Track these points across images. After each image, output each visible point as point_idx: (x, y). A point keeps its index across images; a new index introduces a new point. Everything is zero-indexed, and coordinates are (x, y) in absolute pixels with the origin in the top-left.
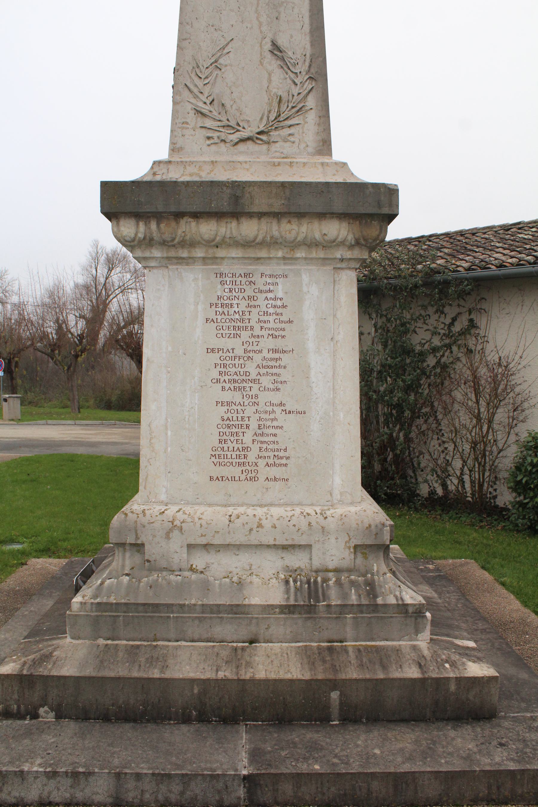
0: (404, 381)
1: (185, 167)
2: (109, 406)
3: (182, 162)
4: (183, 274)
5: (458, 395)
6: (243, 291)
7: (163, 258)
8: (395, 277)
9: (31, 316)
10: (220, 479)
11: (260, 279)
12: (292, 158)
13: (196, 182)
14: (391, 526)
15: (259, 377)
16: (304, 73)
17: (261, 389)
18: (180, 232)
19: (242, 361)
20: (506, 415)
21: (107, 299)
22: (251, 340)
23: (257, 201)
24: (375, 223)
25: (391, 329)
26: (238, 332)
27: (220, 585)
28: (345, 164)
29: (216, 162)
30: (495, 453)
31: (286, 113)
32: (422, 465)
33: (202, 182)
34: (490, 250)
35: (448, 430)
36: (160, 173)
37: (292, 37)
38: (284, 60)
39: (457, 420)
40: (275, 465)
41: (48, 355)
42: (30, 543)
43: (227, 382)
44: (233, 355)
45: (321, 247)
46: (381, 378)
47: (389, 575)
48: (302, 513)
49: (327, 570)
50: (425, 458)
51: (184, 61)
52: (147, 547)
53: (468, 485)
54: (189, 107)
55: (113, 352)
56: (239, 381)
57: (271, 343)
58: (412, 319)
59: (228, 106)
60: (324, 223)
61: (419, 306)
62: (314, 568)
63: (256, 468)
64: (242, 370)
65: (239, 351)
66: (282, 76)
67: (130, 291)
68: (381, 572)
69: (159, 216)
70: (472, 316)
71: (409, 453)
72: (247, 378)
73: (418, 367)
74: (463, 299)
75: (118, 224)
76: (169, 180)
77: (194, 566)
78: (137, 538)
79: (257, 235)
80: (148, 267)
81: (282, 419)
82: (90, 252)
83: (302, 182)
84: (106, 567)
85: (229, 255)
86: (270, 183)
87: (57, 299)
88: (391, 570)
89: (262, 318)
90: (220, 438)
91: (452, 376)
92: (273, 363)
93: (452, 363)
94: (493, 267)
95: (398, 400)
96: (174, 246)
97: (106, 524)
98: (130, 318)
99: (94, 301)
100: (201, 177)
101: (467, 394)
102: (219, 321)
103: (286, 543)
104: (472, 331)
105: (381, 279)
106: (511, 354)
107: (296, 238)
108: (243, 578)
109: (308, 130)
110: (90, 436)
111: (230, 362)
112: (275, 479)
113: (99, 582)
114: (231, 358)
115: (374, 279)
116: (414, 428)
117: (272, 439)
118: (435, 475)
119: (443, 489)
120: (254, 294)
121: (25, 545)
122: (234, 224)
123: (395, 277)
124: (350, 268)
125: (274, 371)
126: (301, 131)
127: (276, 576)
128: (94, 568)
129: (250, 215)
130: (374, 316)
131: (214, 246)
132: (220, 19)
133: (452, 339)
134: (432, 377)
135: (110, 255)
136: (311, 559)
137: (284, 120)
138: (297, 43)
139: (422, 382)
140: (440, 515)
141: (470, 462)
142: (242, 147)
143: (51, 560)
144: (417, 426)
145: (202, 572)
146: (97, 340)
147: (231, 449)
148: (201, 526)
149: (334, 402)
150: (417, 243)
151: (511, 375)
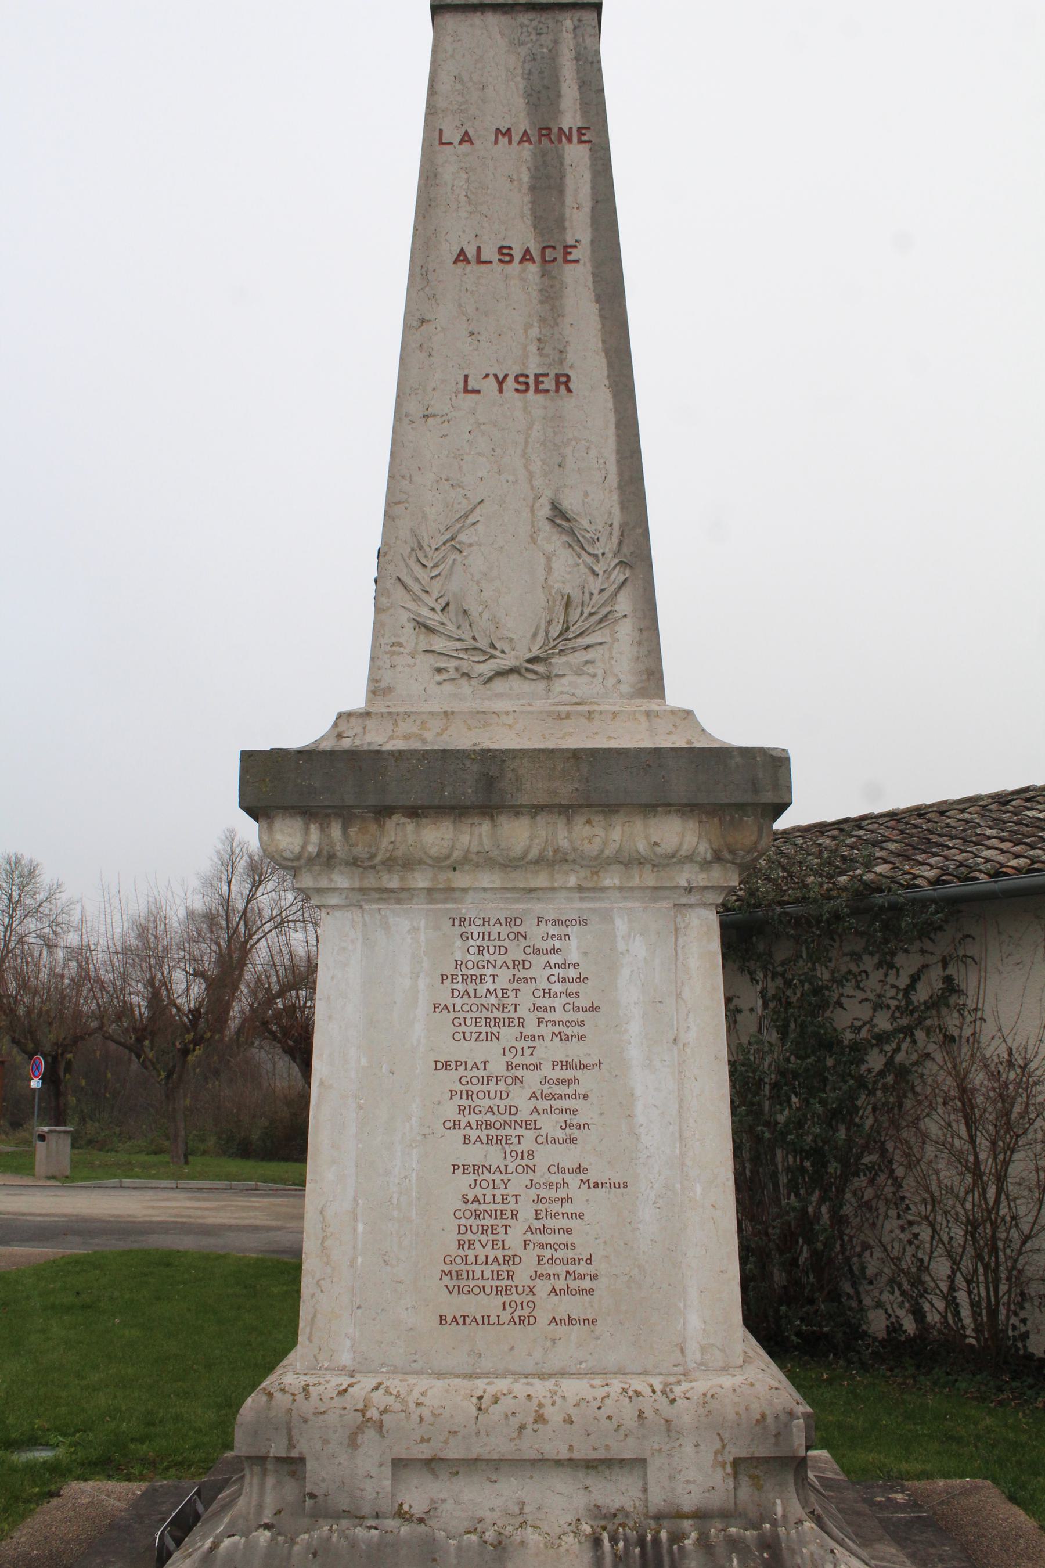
0: (823, 1102)
1: (396, 724)
2: (245, 1151)
3: (390, 713)
4: (391, 920)
5: (932, 1127)
6: (503, 950)
7: (353, 889)
8: (797, 901)
9: (102, 972)
10: (461, 1321)
11: (535, 928)
12: (591, 703)
13: (415, 751)
14: (807, 1416)
15: (535, 1116)
16: (610, 555)
17: (540, 1140)
18: (385, 843)
19: (502, 1086)
20: (1032, 1166)
21: (246, 942)
22: (519, 1045)
23: (528, 784)
24: (749, 820)
25: (794, 999)
26: (495, 1030)
27: (459, 1548)
28: (688, 714)
29: (453, 713)
30: (1016, 1245)
31: (579, 624)
32: (870, 1271)
33: (426, 751)
34: (976, 844)
35: (917, 1199)
36: (350, 733)
37: (586, 495)
38: (574, 533)
39: (934, 1177)
40: (568, 1291)
41: (131, 1050)
42: (70, 1445)
43: (474, 1126)
44: (484, 1073)
45: (649, 866)
46: (779, 1097)
47: (808, 1524)
48: (625, 1390)
49: (681, 1515)
50: (875, 1256)
51: (396, 538)
52: (309, 1466)
53: (965, 1312)
54: (404, 616)
55: (257, 1043)
56: (497, 1125)
57: (557, 1050)
58: (833, 980)
59: (474, 612)
60: (653, 822)
61: (846, 955)
62: (652, 1510)
63: (530, 1298)
64: (502, 1103)
65: (497, 1067)
66: (571, 562)
67: (291, 925)
68: (792, 1520)
69: (346, 815)
70: (951, 971)
71: (842, 1246)
72: (513, 1118)
73: (850, 1075)
74: (930, 939)
75: (270, 828)
76: (365, 748)
77: (406, 1507)
78: (291, 1446)
79: (530, 847)
80: (324, 906)
81: (581, 1198)
82: (218, 852)
83: (610, 750)
84: (227, 1506)
85: (477, 885)
86: (552, 751)
87: (152, 939)
88: (812, 1512)
89: (540, 1002)
90: (460, 1237)
91: (918, 1089)
92: (562, 1089)
93: (916, 1063)
94: (982, 876)
95: (814, 1141)
96: (373, 867)
97: (232, 1405)
98: (291, 977)
99: (222, 943)
100: (424, 741)
101: (950, 1125)
102: (458, 1008)
103: (593, 1455)
104: (953, 999)
105: (769, 905)
106: (1032, 1042)
107: (602, 851)
108: (507, 1533)
109: (621, 653)
110: (206, 1213)
111: (479, 1087)
112: (570, 1321)
113: (208, 1543)
114: (481, 1080)
115: (758, 905)
116: (848, 1196)
117: (562, 1238)
118: (897, 1293)
119: (916, 1320)
120: (525, 957)
121: (60, 1452)
122: (486, 827)
123: (797, 901)
124: (705, 905)
125: (565, 1104)
126: (607, 656)
127: (573, 1527)
128: (200, 1508)
129: (516, 811)
130: (760, 975)
131: (449, 867)
132: (460, 467)
133: (914, 1017)
134: (879, 1093)
135: (256, 858)
136: (645, 1490)
137: (575, 637)
138: (595, 502)
139: (859, 1103)
140: (914, 1377)
141: (967, 1264)
142: (499, 685)
143: (111, 1485)
144: (855, 1194)
145: (421, 1521)
146: (226, 1021)
147: (481, 1259)
148: (421, 1419)
149: (683, 1164)
150: (836, 833)
151: (1035, 1084)
